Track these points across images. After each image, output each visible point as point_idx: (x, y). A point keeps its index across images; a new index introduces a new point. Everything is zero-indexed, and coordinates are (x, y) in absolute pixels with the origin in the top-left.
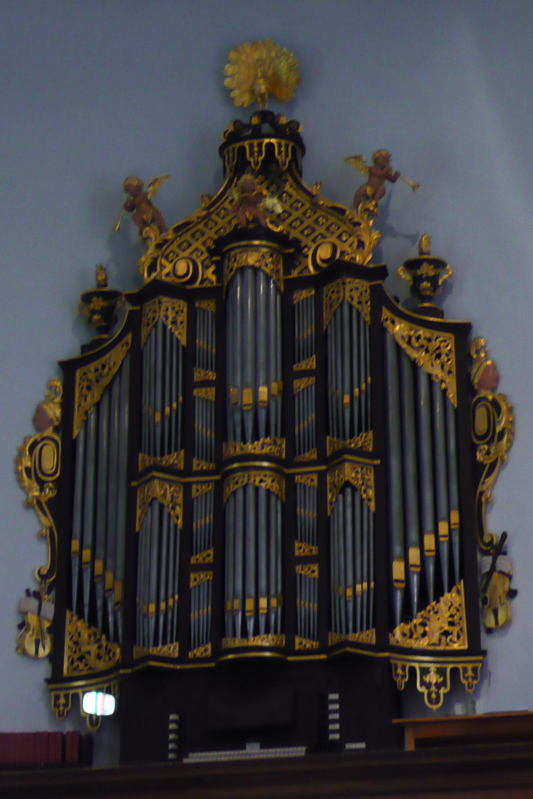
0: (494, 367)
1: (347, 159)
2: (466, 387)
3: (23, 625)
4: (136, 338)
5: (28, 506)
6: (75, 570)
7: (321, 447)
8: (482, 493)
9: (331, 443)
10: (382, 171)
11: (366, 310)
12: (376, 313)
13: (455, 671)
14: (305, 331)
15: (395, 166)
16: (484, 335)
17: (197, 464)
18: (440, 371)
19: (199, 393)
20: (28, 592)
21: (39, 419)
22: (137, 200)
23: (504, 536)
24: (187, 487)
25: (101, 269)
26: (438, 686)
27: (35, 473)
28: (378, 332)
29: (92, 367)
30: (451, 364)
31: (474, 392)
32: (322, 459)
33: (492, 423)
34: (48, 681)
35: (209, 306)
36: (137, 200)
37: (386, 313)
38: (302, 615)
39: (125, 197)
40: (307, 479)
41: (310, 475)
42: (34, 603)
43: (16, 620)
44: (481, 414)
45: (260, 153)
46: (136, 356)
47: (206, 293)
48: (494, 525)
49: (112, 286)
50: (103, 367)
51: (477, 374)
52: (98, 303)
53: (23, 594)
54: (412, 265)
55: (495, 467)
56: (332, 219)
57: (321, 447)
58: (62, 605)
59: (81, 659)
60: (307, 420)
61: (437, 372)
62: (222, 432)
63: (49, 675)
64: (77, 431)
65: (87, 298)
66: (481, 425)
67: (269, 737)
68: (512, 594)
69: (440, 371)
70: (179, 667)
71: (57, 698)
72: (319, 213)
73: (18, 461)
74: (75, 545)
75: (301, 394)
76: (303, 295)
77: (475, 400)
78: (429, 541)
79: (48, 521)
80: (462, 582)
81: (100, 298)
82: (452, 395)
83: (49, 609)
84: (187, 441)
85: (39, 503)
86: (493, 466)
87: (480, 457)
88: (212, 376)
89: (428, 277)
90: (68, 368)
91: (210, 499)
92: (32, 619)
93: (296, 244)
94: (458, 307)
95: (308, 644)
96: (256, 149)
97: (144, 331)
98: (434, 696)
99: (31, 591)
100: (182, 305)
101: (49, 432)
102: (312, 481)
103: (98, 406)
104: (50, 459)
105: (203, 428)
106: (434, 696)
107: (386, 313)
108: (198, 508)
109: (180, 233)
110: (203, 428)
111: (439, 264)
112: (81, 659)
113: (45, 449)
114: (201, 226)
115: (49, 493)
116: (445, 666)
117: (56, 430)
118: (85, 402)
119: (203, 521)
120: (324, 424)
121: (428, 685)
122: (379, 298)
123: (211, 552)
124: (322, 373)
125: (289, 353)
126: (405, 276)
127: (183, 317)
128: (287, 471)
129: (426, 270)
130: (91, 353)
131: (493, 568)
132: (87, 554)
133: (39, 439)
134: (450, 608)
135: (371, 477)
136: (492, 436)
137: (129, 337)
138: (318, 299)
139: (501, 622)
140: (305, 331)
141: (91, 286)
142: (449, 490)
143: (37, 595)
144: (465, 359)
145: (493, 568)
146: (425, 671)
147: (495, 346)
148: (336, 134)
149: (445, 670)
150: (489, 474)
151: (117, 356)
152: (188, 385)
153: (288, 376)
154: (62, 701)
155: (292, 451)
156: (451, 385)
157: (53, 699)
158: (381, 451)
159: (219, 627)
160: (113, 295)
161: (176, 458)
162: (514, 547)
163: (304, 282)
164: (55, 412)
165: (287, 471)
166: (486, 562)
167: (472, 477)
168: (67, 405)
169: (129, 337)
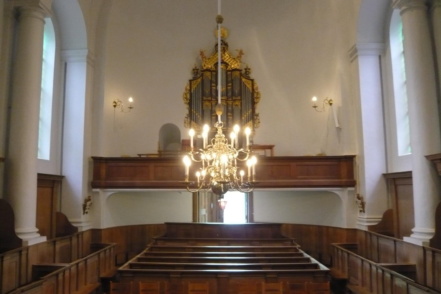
0: (257, 87)
2: (253, 90)
3: (185, 122)
4: (203, 78)
5: (185, 103)
7: (232, 99)
9: (234, 98)
10: (241, 53)
11: (239, 76)
12: (240, 77)
14: (230, 79)
15: (243, 52)
16: (256, 81)
17: (213, 99)
18: (249, 86)
19: (213, 88)
21: (186, 89)
22: (202, 53)
24: (211, 103)
25: (195, 64)
27: (186, 98)
28: (241, 80)
30: (251, 85)
31: (254, 90)
32: (232, 100)
33: (257, 96)
35: (214, 73)
36: (202, 53)
37: (242, 77)
38: (231, 107)
39: (200, 53)
40: (230, 103)
43: (184, 122)
44: (255, 94)
46: (202, 80)
48: (257, 111)
49: (197, 68)
51: (255, 87)
52: (196, 71)
54: (246, 69)
57: (232, 99)
60: (230, 94)
61: (249, 87)
64: (192, 92)
65: (194, 70)
66: (255, 96)
68: (259, 122)
69: (249, 86)
74: (193, 110)
76: (229, 73)
78: (247, 114)
79: (188, 106)
82: (251, 91)
84: (211, 95)
86: (257, 103)
89: (247, 70)
90: (190, 81)
92: (186, 122)
93: (228, 64)
94: (252, 76)
97: (204, 77)
100: (210, 73)
101: (188, 91)
102: (231, 103)
103: (196, 88)
104: (188, 96)
107: (242, 77)
111: (249, 69)
115: (188, 101)
118: (194, 87)
120: (233, 94)
122: (241, 75)
124: (232, 89)
126: (244, 71)
127: (210, 75)
129: (248, 70)
130: (195, 79)
132: (195, 112)
135: (240, 104)
136: (257, 98)
137: (201, 77)
138: (231, 73)
140: (230, 79)
141: (194, 68)
142: (250, 106)
143: (187, 118)
144: (253, 85)
147: (258, 84)
148: (235, 45)
151: (199, 80)
152: (211, 86)
155: (228, 98)
156: (251, 89)
158: (241, 100)
160: (198, 69)
161: (210, 98)
162: (259, 115)
163: (230, 71)
164: (188, 88)
166: (255, 117)
167: (254, 103)
168: (191, 87)
169: (201, 77)
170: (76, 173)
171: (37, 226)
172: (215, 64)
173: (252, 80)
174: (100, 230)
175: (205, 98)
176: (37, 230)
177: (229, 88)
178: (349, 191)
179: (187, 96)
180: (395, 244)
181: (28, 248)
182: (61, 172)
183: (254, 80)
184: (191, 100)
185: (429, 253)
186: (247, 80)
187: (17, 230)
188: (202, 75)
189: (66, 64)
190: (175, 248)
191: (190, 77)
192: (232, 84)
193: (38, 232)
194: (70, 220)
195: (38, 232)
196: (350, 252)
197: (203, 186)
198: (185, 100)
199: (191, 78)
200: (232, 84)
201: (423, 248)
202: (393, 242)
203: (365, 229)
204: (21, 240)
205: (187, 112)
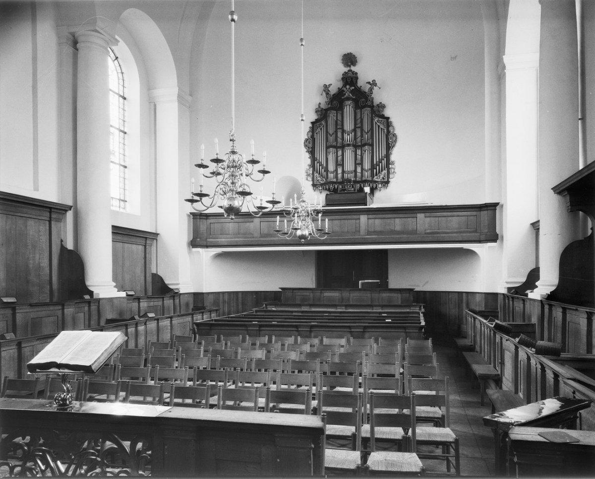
90: (313, 123)
166: (390, 166)
170: (173, 229)
171: (113, 281)
173: (388, 118)
174: (202, 294)
176: (115, 284)
178: (489, 247)
180: (524, 304)
181: (99, 300)
182: (156, 230)
185: (546, 307)
187: (88, 283)
189: (155, 105)
191: (313, 117)
193: (115, 287)
194: (166, 282)
195: (115, 287)
196: (475, 315)
201: (541, 301)
202: (522, 302)
203: (504, 291)
204: (93, 292)
205: (309, 161)
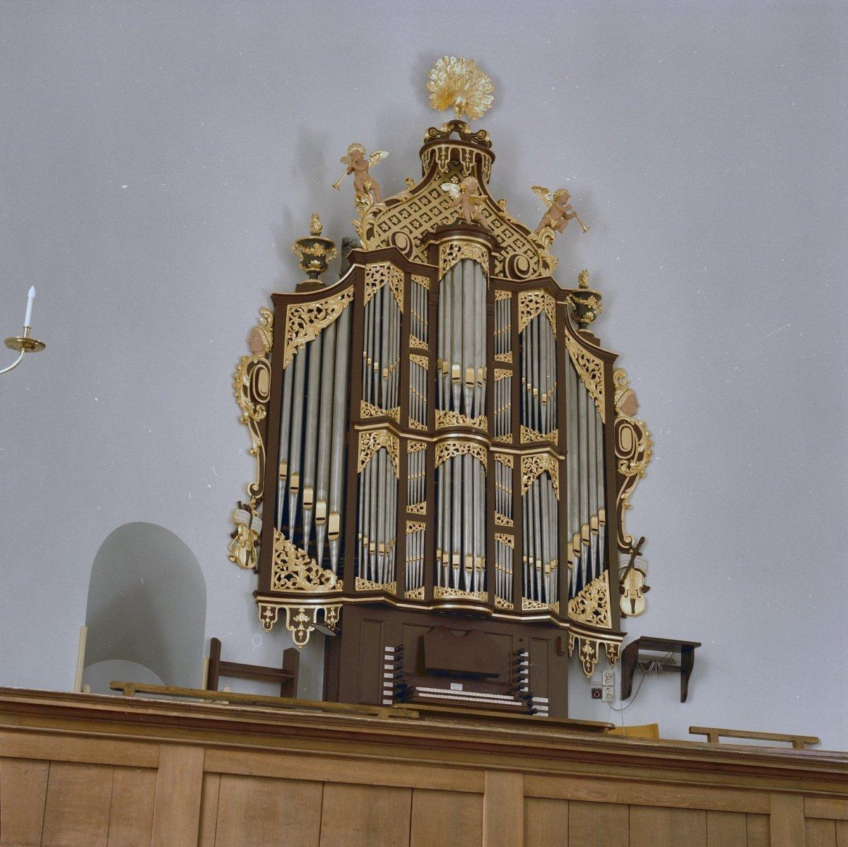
1: (533, 188)
2: (611, 410)
5: (244, 422)
6: (281, 493)
7: (517, 437)
8: (622, 500)
13: (321, 612)
17: (413, 424)
20: (240, 505)
23: (642, 540)
24: (404, 441)
26: (306, 625)
27: (252, 392)
29: (305, 306)
34: (256, 594)
41: (507, 456)
42: (243, 516)
45: (447, 158)
46: (356, 308)
47: (420, 270)
48: (632, 528)
50: (319, 310)
53: (235, 506)
55: (632, 484)
56: (516, 236)
58: (269, 521)
59: (289, 577)
60: (504, 407)
62: (434, 400)
63: (255, 587)
64: (287, 362)
65: (306, 243)
67: (472, 679)
70: (431, 608)
71: (264, 609)
72: (505, 226)
73: (236, 379)
75: (499, 383)
77: (616, 421)
79: (257, 441)
80: (607, 572)
81: (322, 246)
83: (257, 524)
85: (252, 420)
86: (633, 479)
87: (623, 470)
88: (424, 346)
91: (422, 456)
95: (506, 605)
96: (443, 153)
98: (301, 634)
99: (243, 503)
104: (264, 386)
105: (417, 392)
106: (301, 634)
108: (412, 461)
109: (391, 207)
110: (417, 392)
112: (289, 577)
113: (262, 373)
114: (406, 206)
116: (312, 607)
117: (267, 356)
119: (416, 475)
120: (522, 412)
121: (296, 624)
123: (424, 504)
125: (491, 348)
128: (402, 435)
129: (591, 302)
131: (631, 564)
133: (256, 362)
134: (598, 593)
137: (350, 290)
139: (637, 610)
140: (503, 330)
143: (247, 508)
145: (631, 564)
146: (295, 613)
149: (595, 643)
150: (629, 486)
151: (338, 305)
153: (491, 364)
154: (268, 614)
157: (260, 611)
159: (431, 576)
161: (396, 413)
164: (267, 339)
165: (402, 435)
166: (624, 559)
169: (350, 290)
172: (426, 237)
173: (609, 359)
175: (367, 409)
177: (500, 374)
179: (255, 380)
183: (618, 364)
184: (274, 406)
186: (588, 355)
188: (358, 280)
190: (581, 761)
192: (519, 357)
197: (585, 640)
198: (245, 400)
199: (290, 290)
200: (519, 357)
